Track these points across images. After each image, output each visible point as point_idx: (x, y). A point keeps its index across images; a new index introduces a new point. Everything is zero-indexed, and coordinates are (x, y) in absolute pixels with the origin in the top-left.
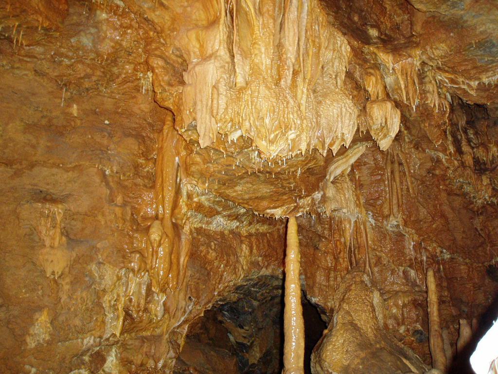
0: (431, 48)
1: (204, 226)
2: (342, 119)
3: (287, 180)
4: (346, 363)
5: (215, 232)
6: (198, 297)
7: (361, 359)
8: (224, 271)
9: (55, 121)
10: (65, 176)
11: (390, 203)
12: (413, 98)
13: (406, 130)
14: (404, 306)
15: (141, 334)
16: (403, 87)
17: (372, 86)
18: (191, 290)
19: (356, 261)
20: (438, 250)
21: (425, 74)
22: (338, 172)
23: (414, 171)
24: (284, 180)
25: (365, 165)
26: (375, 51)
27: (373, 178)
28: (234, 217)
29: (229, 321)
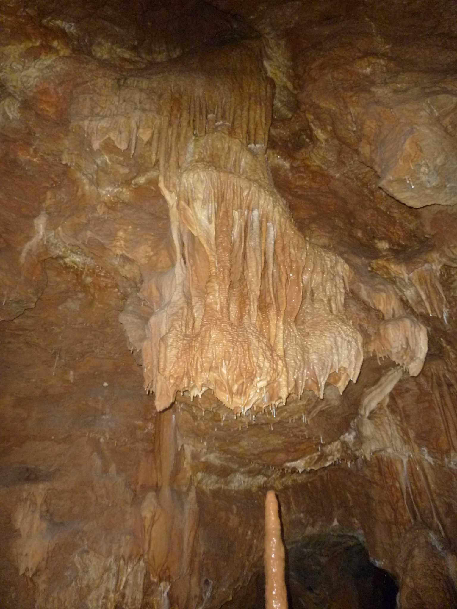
0: (449, 248)
1: (223, 486)
2: (337, 350)
3: (297, 427)
5: (237, 492)
8: (253, 539)
11: (447, 435)
12: (439, 308)
13: (448, 345)
16: (424, 297)
17: (386, 303)
18: (208, 570)
19: (420, 513)
21: (453, 279)
22: (374, 405)
24: (293, 428)
25: (407, 392)
26: (385, 264)
28: (256, 473)
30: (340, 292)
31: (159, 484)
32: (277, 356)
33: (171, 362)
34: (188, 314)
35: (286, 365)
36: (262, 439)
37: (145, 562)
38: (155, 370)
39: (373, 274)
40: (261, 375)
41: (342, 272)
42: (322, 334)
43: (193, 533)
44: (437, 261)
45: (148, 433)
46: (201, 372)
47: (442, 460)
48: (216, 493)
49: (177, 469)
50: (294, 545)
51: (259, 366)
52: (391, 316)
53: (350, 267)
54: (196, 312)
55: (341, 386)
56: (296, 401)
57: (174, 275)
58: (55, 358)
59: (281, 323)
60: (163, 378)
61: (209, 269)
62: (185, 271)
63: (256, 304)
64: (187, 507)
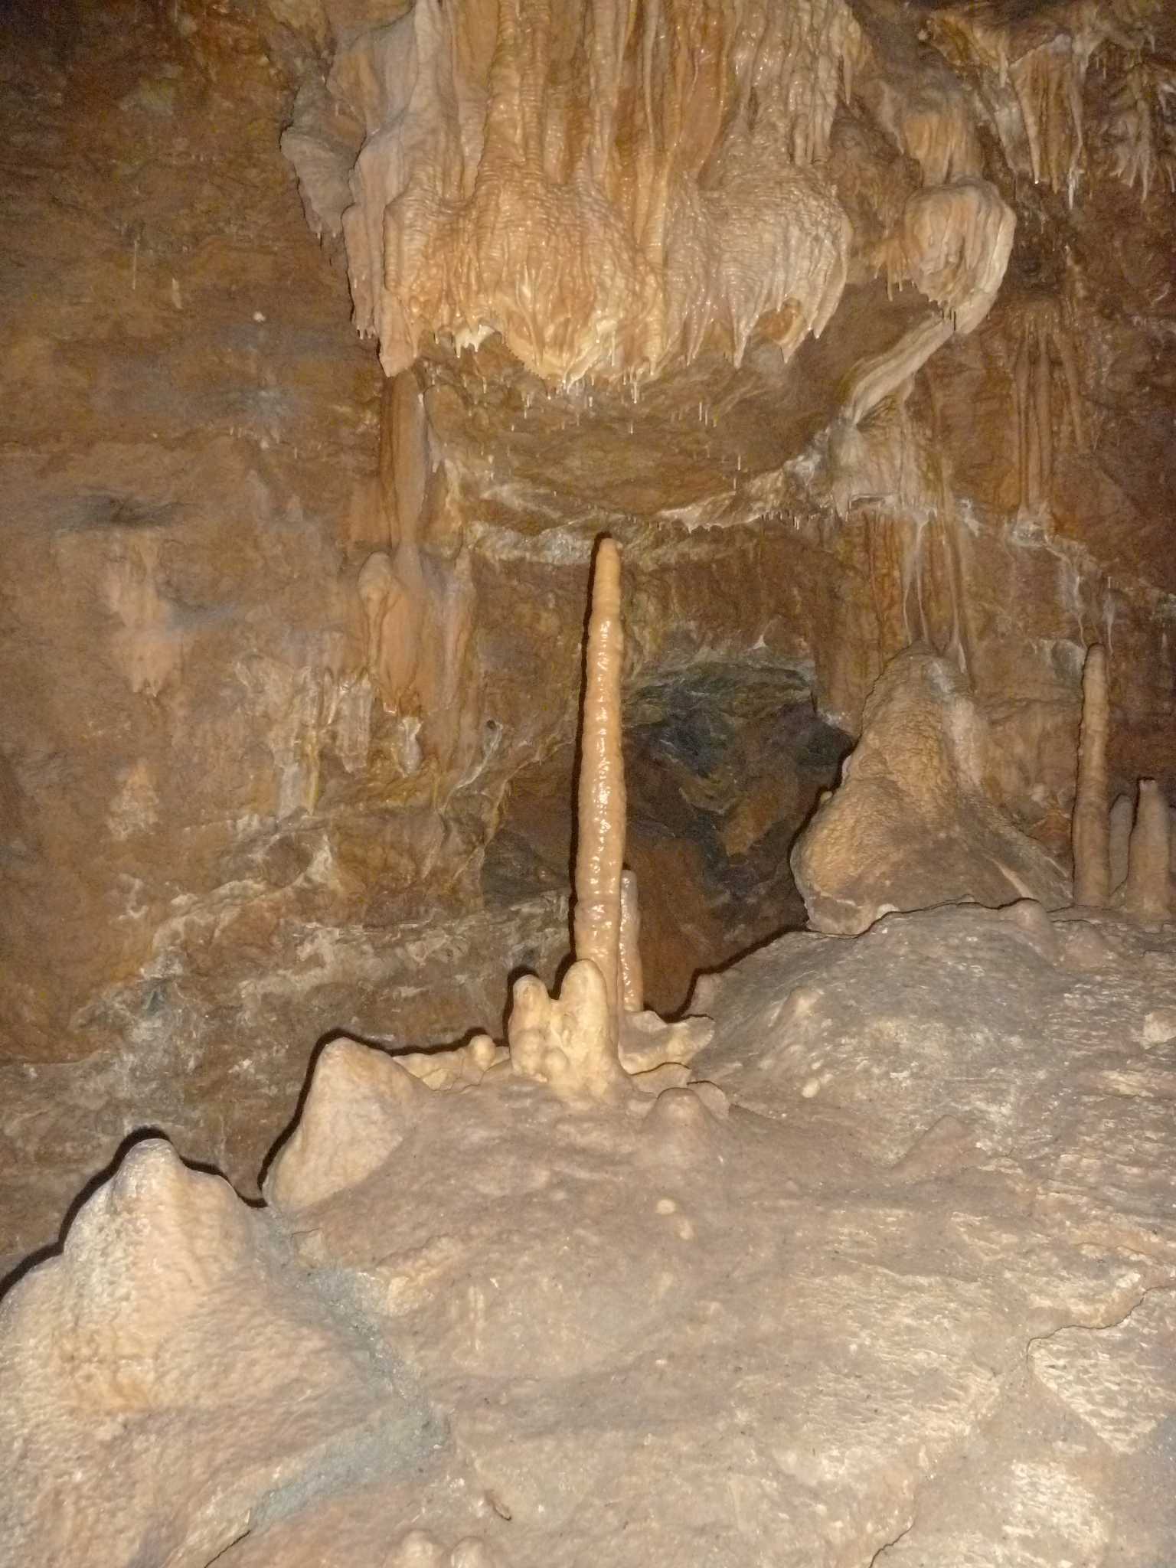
3: (686, 434)
4: (852, 872)
6: (513, 721)
7: (894, 864)
9: (131, 329)
10: (167, 460)
12: (1059, 165)
13: (1077, 262)
14: (1045, 736)
15: (383, 805)
17: (938, 142)
20: (1155, 593)
22: (874, 398)
23: (1098, 383)
26: (962, 24)
27: (982, 408)
29: (675, 761)
30: (826, 105)
31: (394, 540)
32: (647, 263)
33: (413, 267)
34: (447, 149)
35: (665, 286)
36: (610, 457)
37: (373, 681)
38: (377, 282)
39: (925, 54)
40: (605, 306)
41: (841, 46)
42: (758, 217)
43: (464, 637)
44: (1088, 30)
45: (363, 435)
46: (478, 292)
47: (998, 524)
48: (513, 568)
49: (430, 514)
50: (670, 681)
51: (602, 285)
52: (941, 176)
53: (864, 31)
54: (468, 141)
55: (789, 344)
56: (686, 373)
57: (413, 40)
58: (131, 245)
59: (663, 183)
60: (395, 304)
61: (500, 24)
62: (439, 26)
63: (607, 131)
64: (452, 587)
